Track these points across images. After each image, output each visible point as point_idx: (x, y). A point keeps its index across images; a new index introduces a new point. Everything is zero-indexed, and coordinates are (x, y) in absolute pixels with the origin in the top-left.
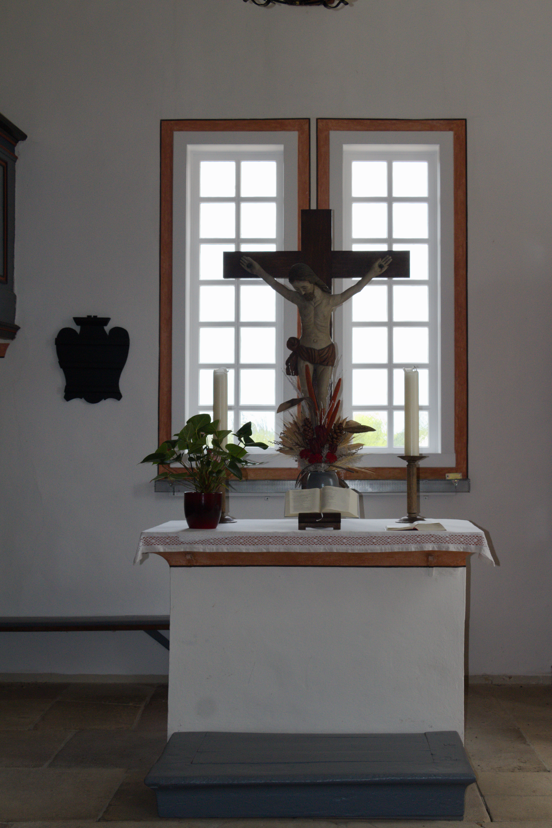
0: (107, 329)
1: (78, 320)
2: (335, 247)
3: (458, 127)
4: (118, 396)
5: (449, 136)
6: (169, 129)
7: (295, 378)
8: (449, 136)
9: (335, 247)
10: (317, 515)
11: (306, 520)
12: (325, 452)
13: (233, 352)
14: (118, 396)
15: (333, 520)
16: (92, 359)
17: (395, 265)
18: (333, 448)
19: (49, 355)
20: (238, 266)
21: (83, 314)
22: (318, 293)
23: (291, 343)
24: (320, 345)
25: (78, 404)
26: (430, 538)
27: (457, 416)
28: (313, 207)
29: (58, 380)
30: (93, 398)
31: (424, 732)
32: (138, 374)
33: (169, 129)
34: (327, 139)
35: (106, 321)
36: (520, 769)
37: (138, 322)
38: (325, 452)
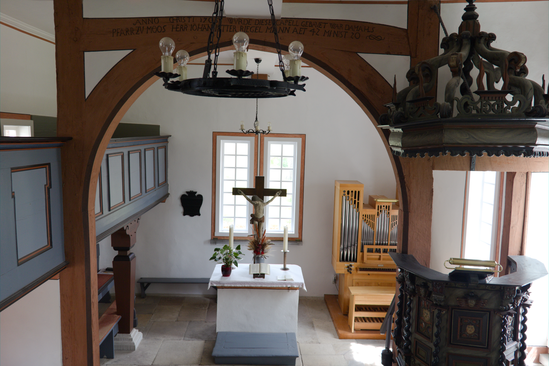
0: (196, 195)
1: (187, 192)
2: (265, 188)
3: (303, 137)
4: (199, 215)
5: (300, 139)
6: (215, 135)
7: (252, 225)
8: (300, 139)
9: (265, 188)
10: (258, 274)
11: (255, 276)
12: (261, 252)
13: (233, 217)
14: (199, 215)
15: (263, 276)
16: (192, 204)
17: (283, 193)
18: (263, 250)
19: (179, 202)
20: (236, 191)
21: (189, 190)
22: (260, 203)
23: (252, 215)
24: (261, 217)
25: (187, 217)
26: (289, 283)
27: (299, 223)
28: (258, 175)
29: (181, 209)
30: (192, 215)
31: (285, 332)
32: (205, 208)
33: (215, 135)
34: (263, 139)
35: (196, 193)
36: (312, 342)
37: (205, 192)
38: (261, 252)
